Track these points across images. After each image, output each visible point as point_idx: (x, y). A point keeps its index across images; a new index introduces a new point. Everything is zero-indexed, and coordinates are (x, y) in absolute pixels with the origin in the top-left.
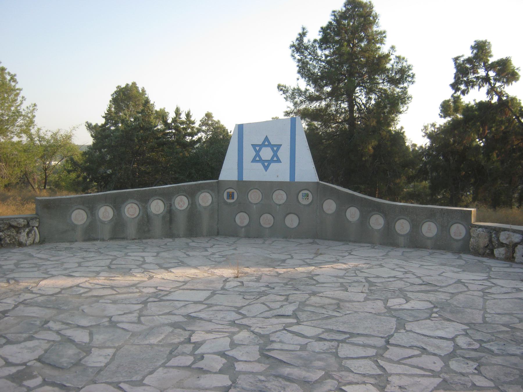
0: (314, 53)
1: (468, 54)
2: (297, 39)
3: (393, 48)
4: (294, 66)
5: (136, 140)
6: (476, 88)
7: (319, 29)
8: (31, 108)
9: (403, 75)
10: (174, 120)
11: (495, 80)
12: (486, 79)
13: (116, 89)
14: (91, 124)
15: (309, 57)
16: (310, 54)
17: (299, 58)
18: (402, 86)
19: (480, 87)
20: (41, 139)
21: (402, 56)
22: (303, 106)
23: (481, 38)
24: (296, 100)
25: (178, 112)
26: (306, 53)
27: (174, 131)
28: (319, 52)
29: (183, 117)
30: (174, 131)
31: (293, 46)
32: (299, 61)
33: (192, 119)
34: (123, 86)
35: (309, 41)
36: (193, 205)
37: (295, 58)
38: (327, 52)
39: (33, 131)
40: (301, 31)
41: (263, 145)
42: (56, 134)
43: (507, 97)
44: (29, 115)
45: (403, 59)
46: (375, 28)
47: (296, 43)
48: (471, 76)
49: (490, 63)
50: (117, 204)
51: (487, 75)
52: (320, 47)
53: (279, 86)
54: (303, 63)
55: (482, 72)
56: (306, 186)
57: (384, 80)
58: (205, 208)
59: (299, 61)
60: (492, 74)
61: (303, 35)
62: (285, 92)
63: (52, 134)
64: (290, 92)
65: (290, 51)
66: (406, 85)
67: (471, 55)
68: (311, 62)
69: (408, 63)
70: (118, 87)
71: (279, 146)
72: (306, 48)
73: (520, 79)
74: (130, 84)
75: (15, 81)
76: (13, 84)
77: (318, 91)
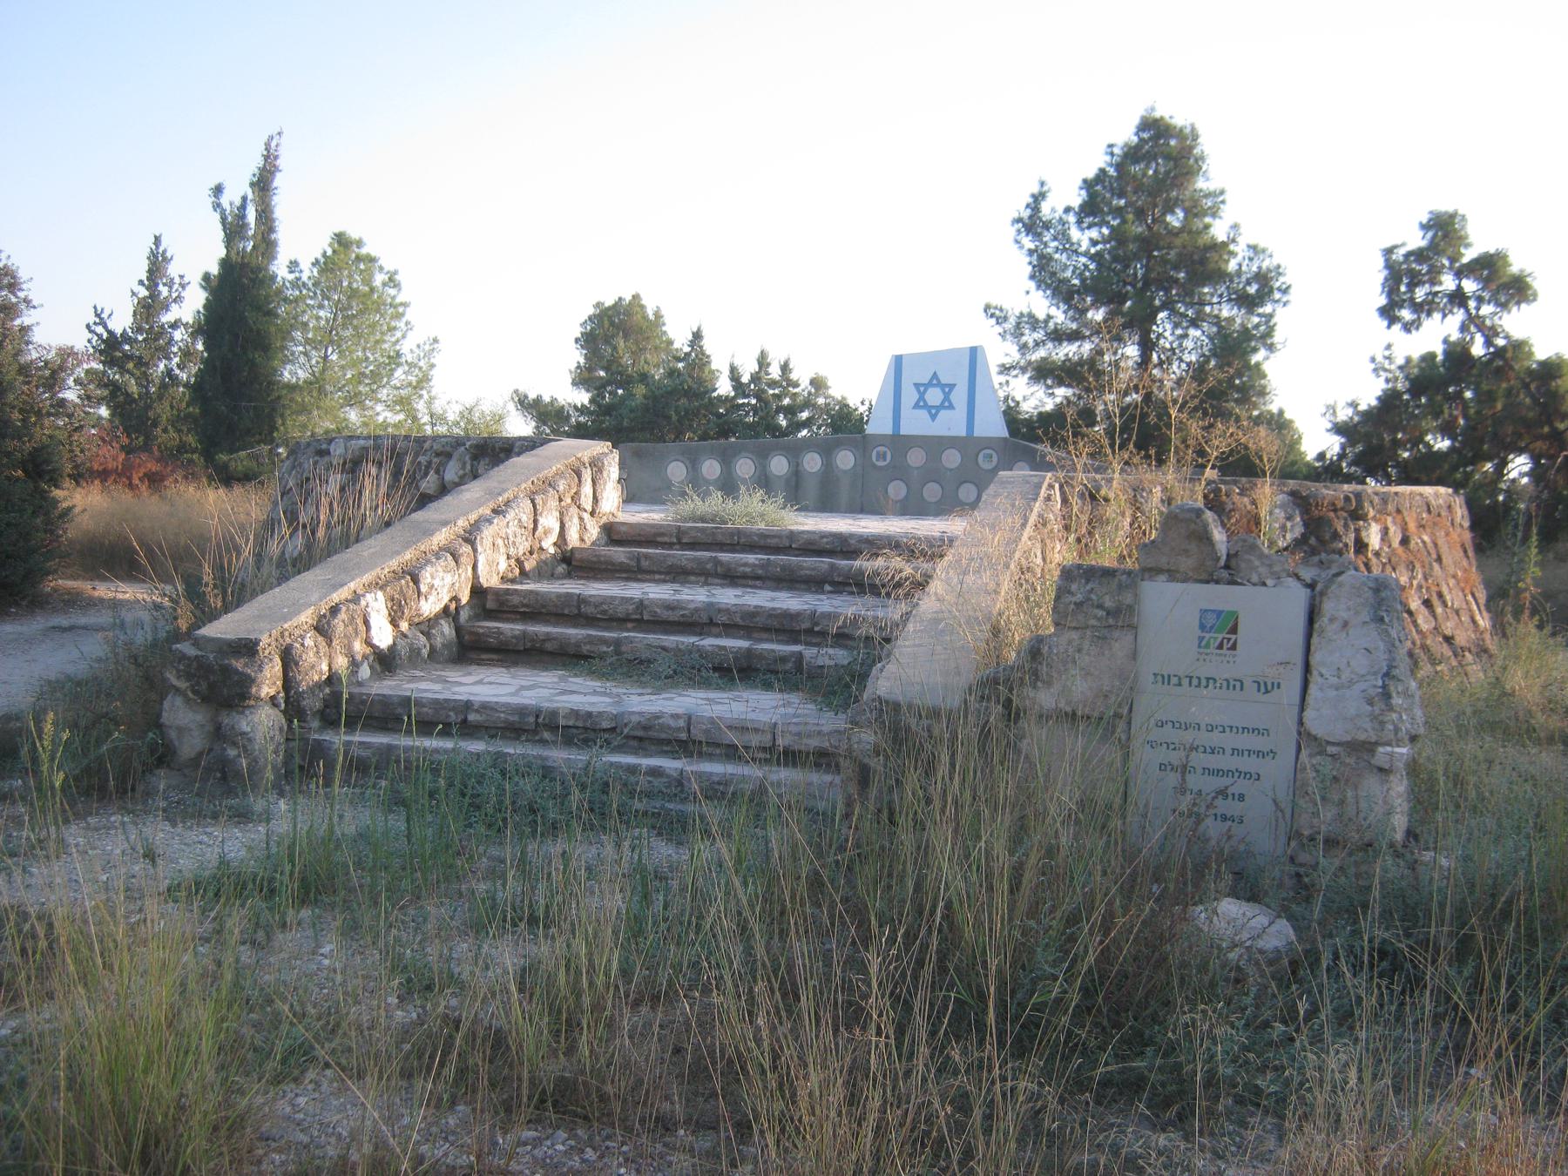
0: (1063, 236)
1: (1417, 240)
2: (1028, 206)
3: (1235, 227)
4: (1022, 266)
5: (674, 418)
6: (1437, 316)
7: (1079, 183)
8: (427, 347)
9: (1262, 289)
10: (755, 378)
11: (1480, 300)
12: (1458, 298)
13: (591, 311)
14: (526, 397)
15: (1055, 244)
16: (1055, 239)
17: (1032, 246)
18: (1261, 310)
19: (1444, 316)
20: (436, 418)
21: (1262, 245)
22: (1042, 353)
23: (1445, 206)
24: (1024, 339)
25: (763, 361)
26: (1047, 237)
27: (754, 401)
28: (1075, 234)
29: (775, 372)
30: (754, 401)
31: (1019, 220)
32: (1031, 252)
33: (794, 376)
34: (609, 302)
35: (1053, 210)
36: (828, 465)
37: (1022, 247)
38: (1094, 233)
39: (421, 406)
40: (1036, 190)
41: (939, 408)
42: (470, 411)
43: (1507, 337)
44: (422, 364)
45: (1264, 251)
46: (1201, 184)
47: (1026, 214)
48: (1420, 293)
49: (1465, 260)
50: (727, 459)
51: (1459, 288)
52: (1079, 222)
53: (987, 308)
54: (1042, 257)
55: (1448, 283)
56: (988, 443)
57: (1221, 296)
58: (845, 472)
59: (1031, 252)
60: (1470, 286)
61: (1038, 198)
62: (1001, 320)
63: (461, 408)
64: (1012, 320)
65: (1012, 231)
66: (1268, 309)
67: (1423, 243)
68: (1057, 256)
69: (1275, 262)
70: (598, 305)
71: (952, 387)
72: (1047, 226)
73: (1540, 298)
74: (628, 298)
75: (397, 286)
76: (392, 292)
77: (1073, 319)
